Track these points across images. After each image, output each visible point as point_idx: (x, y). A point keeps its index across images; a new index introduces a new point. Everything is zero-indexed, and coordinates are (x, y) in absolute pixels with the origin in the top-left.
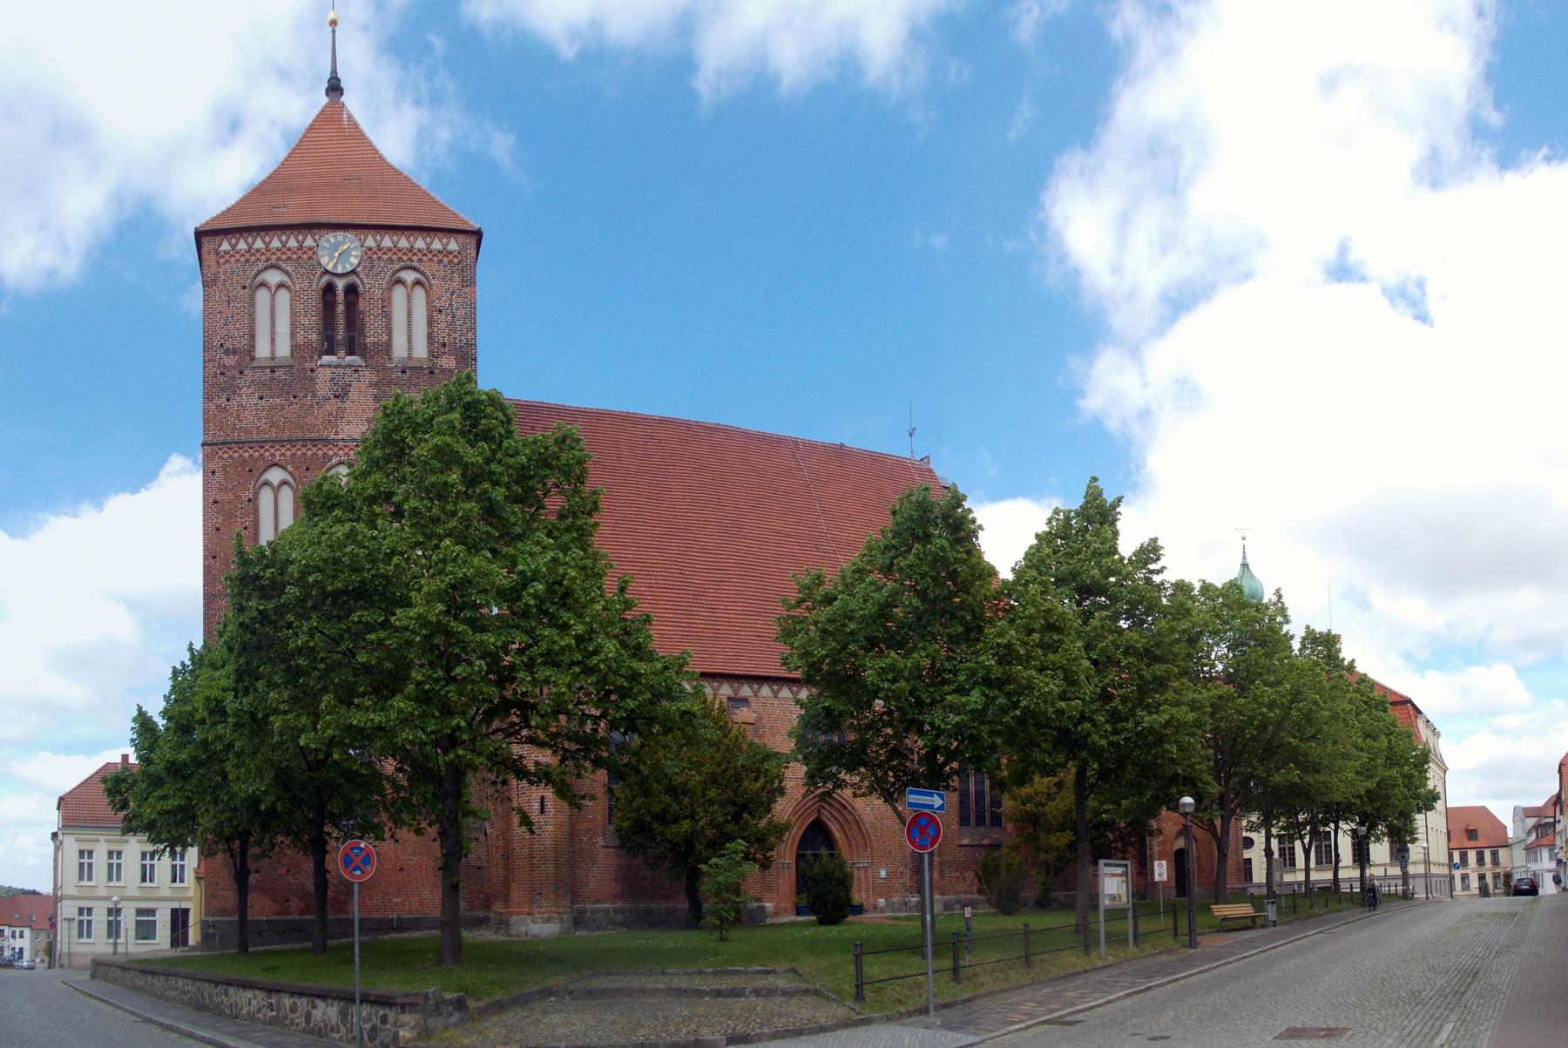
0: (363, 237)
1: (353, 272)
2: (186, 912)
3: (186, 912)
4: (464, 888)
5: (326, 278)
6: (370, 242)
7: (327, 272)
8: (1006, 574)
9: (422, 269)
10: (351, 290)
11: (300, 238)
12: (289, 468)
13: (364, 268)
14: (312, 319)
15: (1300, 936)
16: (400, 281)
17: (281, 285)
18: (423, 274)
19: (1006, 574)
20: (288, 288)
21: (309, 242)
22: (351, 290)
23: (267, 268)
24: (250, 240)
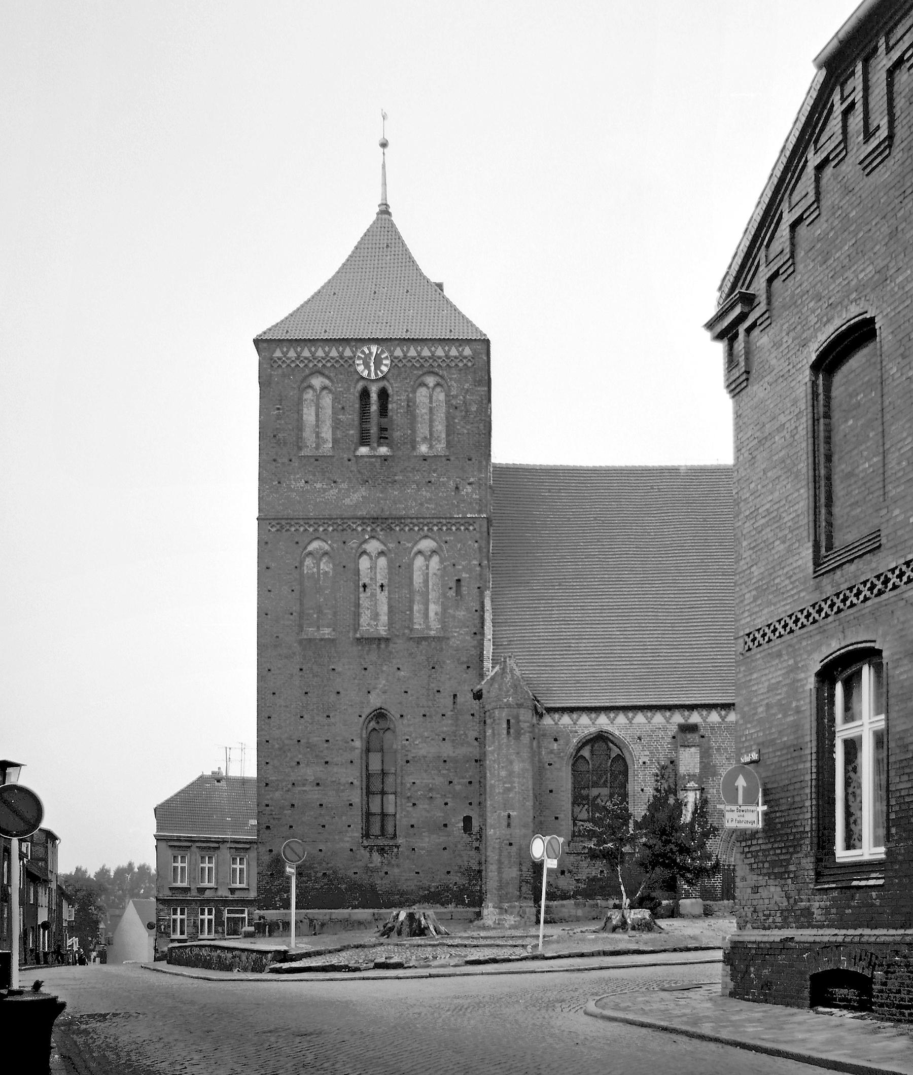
0: (313, 349)
1: (384, 378)
2: (212, 920)
3: (212, 920)
4: (492, 752)
5: (360, 386)
6: (398, 352)
7: (363, 378)
8: (741, 776)
9: (441, 373)
10: (383, 395)
11: (299, 349)
12: (329, 542)
13: (393, 374)
14: (352, 416)
15: (842, 651)
16: (424, 385)
17: (324, 388)
18: (442, 377)
19: (741, 776)
20: (330, 391)
21: (348, 353)
22: (383, 395)
23: (312, 374)
24: (327, 349)
